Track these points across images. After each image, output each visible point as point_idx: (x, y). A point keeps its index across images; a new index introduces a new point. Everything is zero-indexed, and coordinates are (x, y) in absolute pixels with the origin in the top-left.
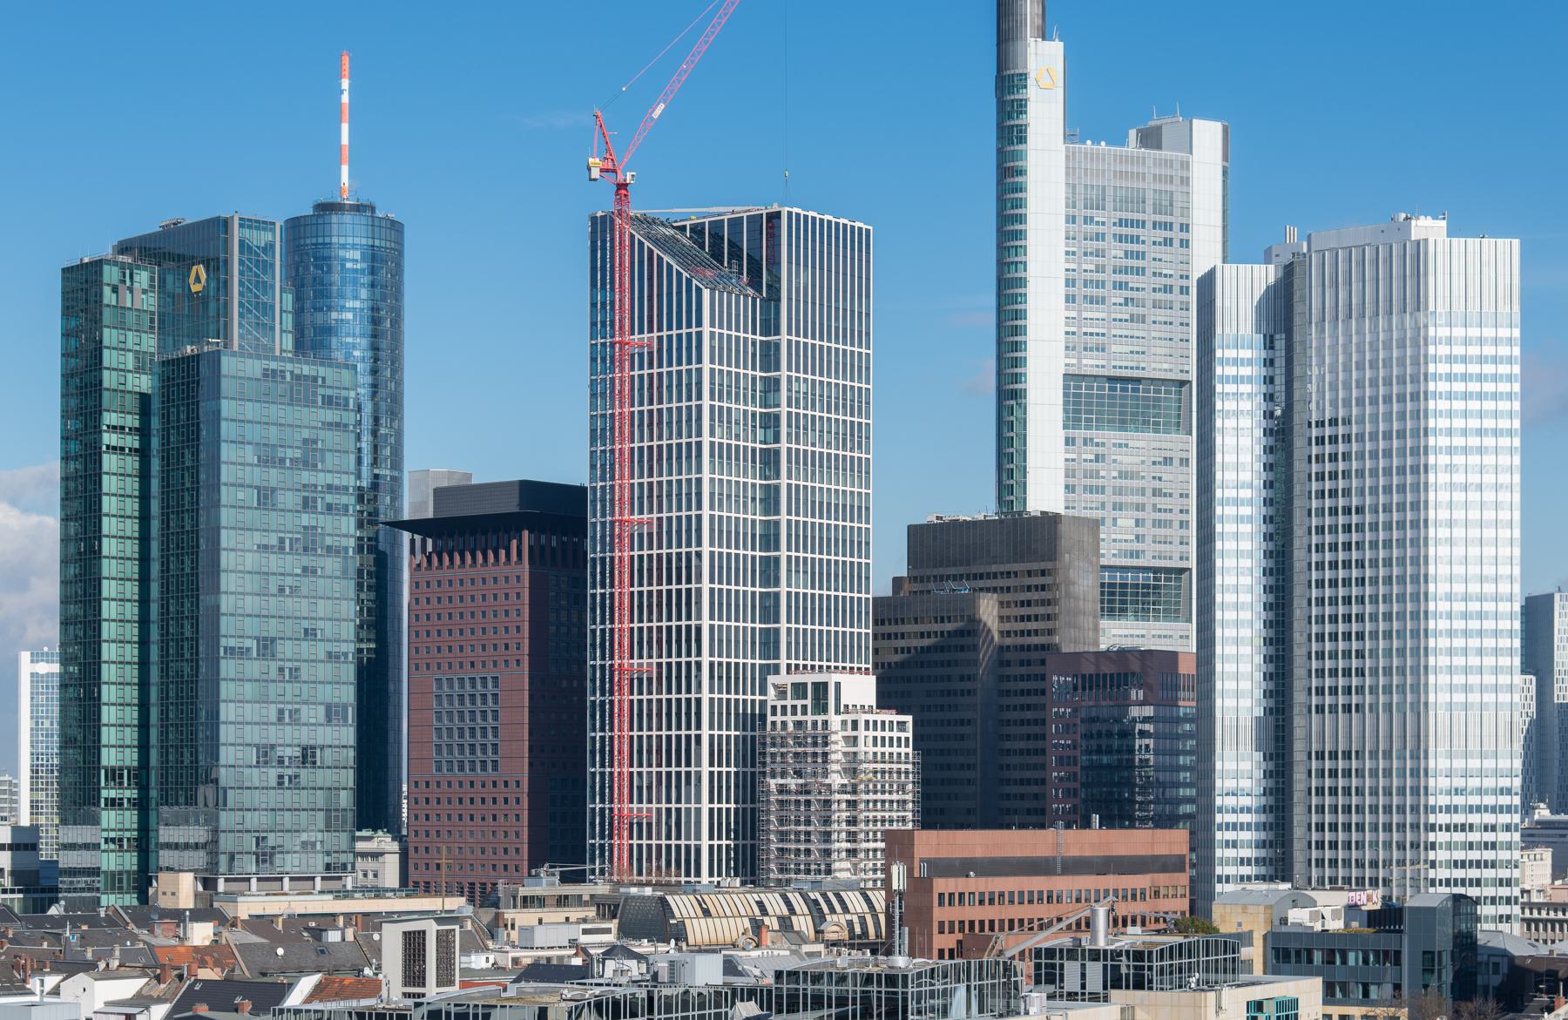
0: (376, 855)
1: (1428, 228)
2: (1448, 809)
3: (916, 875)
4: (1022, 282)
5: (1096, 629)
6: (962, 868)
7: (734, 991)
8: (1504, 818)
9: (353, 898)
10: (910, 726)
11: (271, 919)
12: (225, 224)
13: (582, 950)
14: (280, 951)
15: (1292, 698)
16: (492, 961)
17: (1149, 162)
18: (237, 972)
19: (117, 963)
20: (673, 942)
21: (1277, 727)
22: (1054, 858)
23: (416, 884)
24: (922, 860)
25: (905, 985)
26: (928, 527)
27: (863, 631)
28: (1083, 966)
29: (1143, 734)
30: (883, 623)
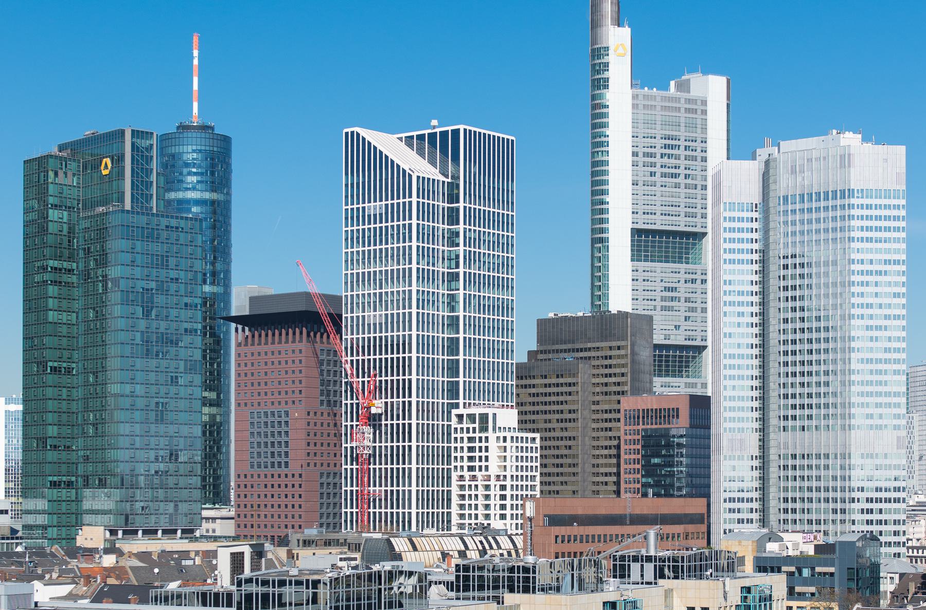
5: (651, 382)
10: (538, 441)
11: (150, 553)
24: (545, 516)
28: (642, 566)
29: (680, 445)
30: (522, 378)
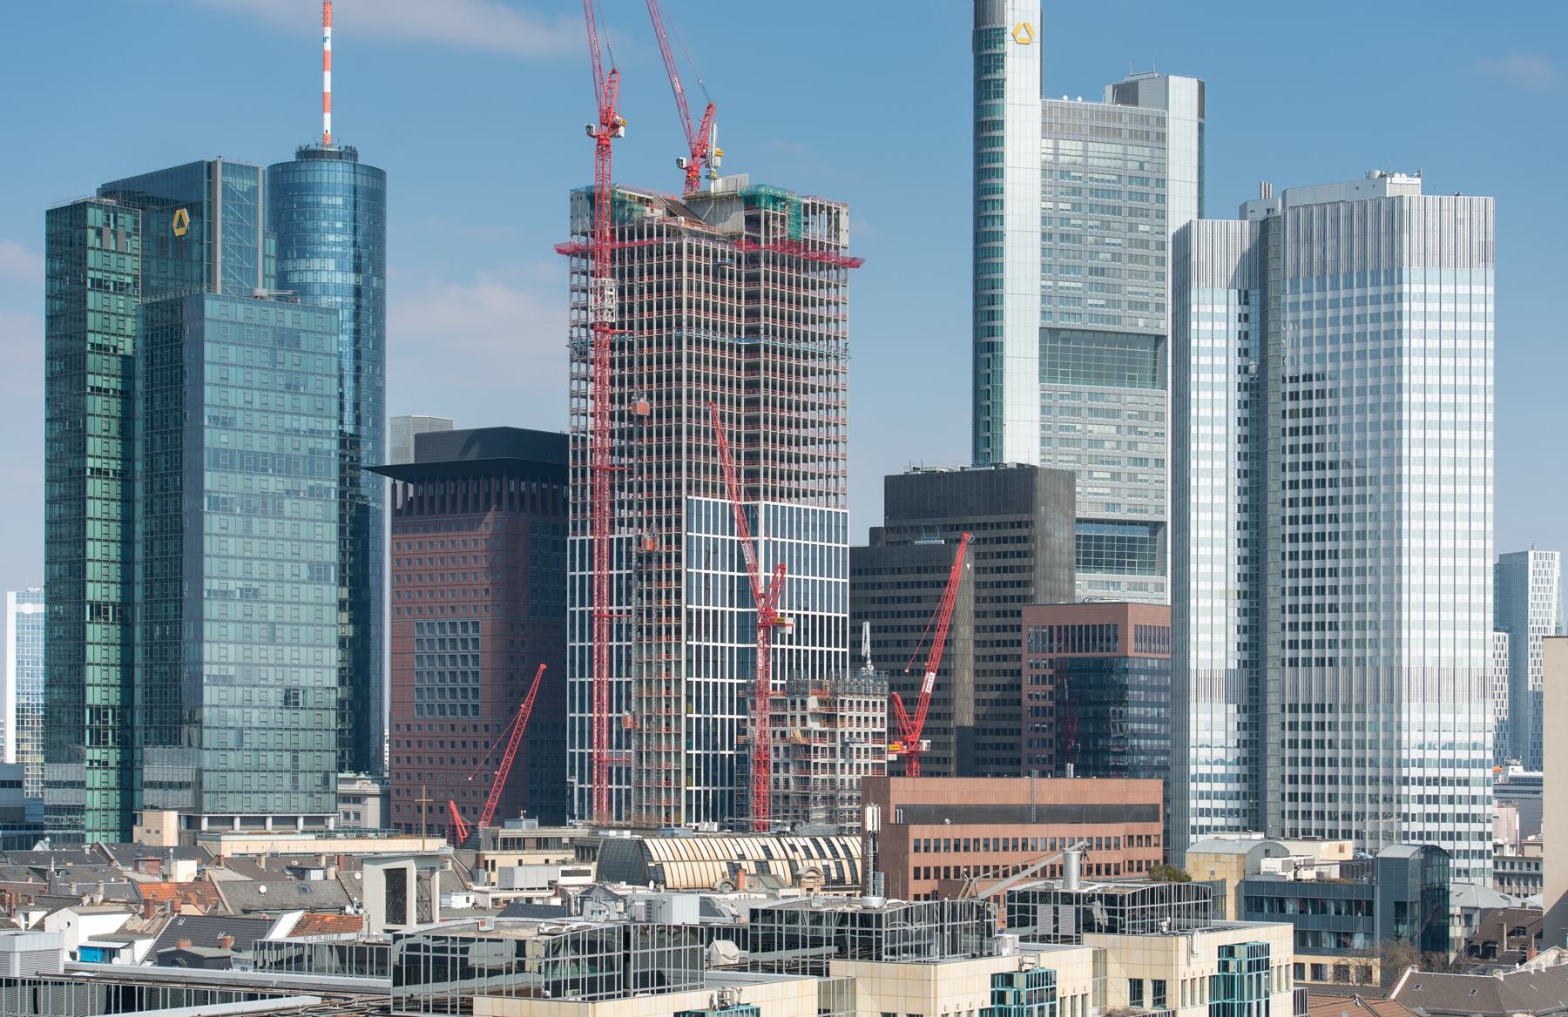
0: (358, 798)
1: (1403, 185)
2: (1421, 763)
3: (892, 821)
4: (999, 236)
5: (1072, 581)
6: (938, 814)
7: (711, 930)
8: (1477, 773)
9: (335, 838)
12: (211, 167)
13: (561, 891)
14: (263, 889)
15: (1265, 652)
16: (472, 900)
17: (1125, 118)
18: (221, 908)
19: (101, 898)
20: (652, 884)
21: (1251, 680)
22: (1030, 806)
23: (398, 825)
24: (898, 807)
25: (879, 925)
26: (905, 478)
27: (840, 650)
28: (1056, 910)
30: (860, 573)
